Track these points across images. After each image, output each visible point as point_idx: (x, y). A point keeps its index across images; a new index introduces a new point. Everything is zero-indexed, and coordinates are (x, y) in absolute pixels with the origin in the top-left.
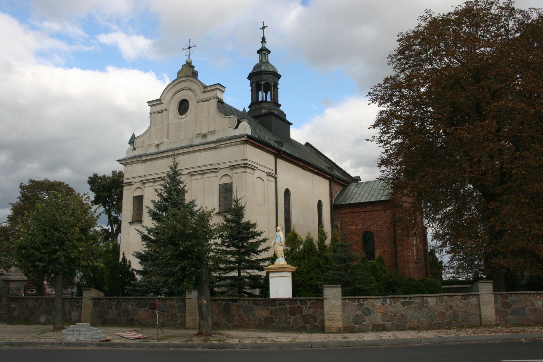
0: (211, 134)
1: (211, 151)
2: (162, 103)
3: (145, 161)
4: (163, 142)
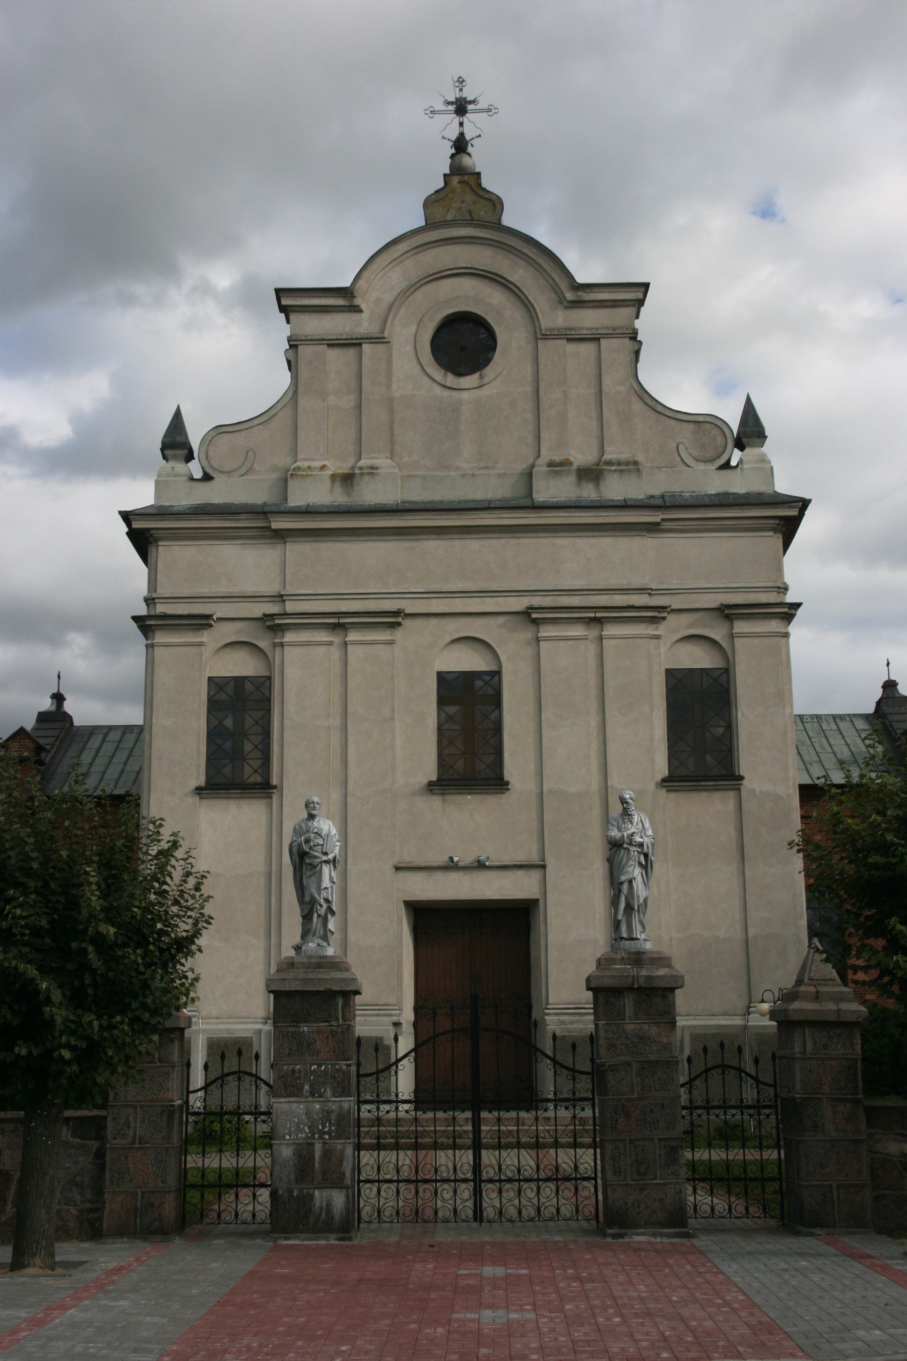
0: (622, 471)
1: (626, 540)
2: (357, 310)
3: (281, 536)
4: (372, 468)
